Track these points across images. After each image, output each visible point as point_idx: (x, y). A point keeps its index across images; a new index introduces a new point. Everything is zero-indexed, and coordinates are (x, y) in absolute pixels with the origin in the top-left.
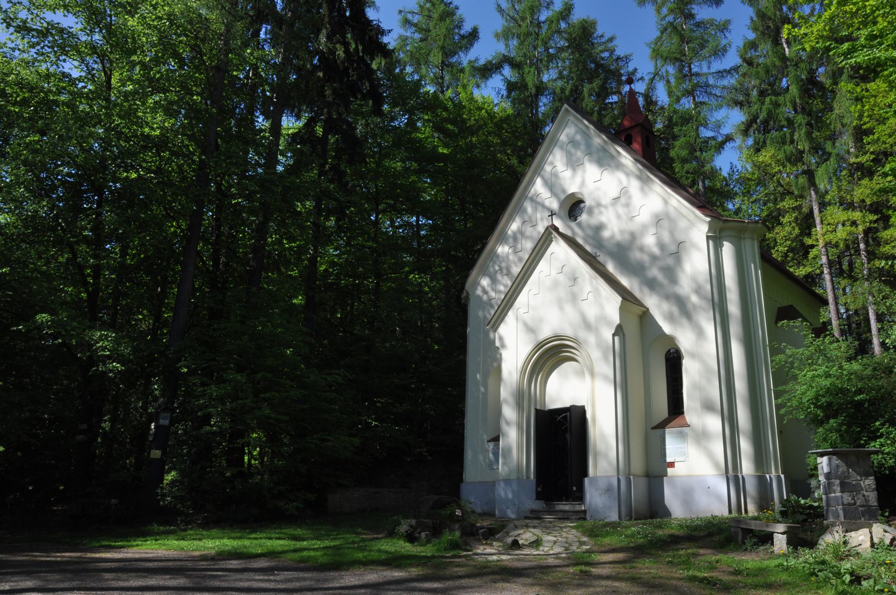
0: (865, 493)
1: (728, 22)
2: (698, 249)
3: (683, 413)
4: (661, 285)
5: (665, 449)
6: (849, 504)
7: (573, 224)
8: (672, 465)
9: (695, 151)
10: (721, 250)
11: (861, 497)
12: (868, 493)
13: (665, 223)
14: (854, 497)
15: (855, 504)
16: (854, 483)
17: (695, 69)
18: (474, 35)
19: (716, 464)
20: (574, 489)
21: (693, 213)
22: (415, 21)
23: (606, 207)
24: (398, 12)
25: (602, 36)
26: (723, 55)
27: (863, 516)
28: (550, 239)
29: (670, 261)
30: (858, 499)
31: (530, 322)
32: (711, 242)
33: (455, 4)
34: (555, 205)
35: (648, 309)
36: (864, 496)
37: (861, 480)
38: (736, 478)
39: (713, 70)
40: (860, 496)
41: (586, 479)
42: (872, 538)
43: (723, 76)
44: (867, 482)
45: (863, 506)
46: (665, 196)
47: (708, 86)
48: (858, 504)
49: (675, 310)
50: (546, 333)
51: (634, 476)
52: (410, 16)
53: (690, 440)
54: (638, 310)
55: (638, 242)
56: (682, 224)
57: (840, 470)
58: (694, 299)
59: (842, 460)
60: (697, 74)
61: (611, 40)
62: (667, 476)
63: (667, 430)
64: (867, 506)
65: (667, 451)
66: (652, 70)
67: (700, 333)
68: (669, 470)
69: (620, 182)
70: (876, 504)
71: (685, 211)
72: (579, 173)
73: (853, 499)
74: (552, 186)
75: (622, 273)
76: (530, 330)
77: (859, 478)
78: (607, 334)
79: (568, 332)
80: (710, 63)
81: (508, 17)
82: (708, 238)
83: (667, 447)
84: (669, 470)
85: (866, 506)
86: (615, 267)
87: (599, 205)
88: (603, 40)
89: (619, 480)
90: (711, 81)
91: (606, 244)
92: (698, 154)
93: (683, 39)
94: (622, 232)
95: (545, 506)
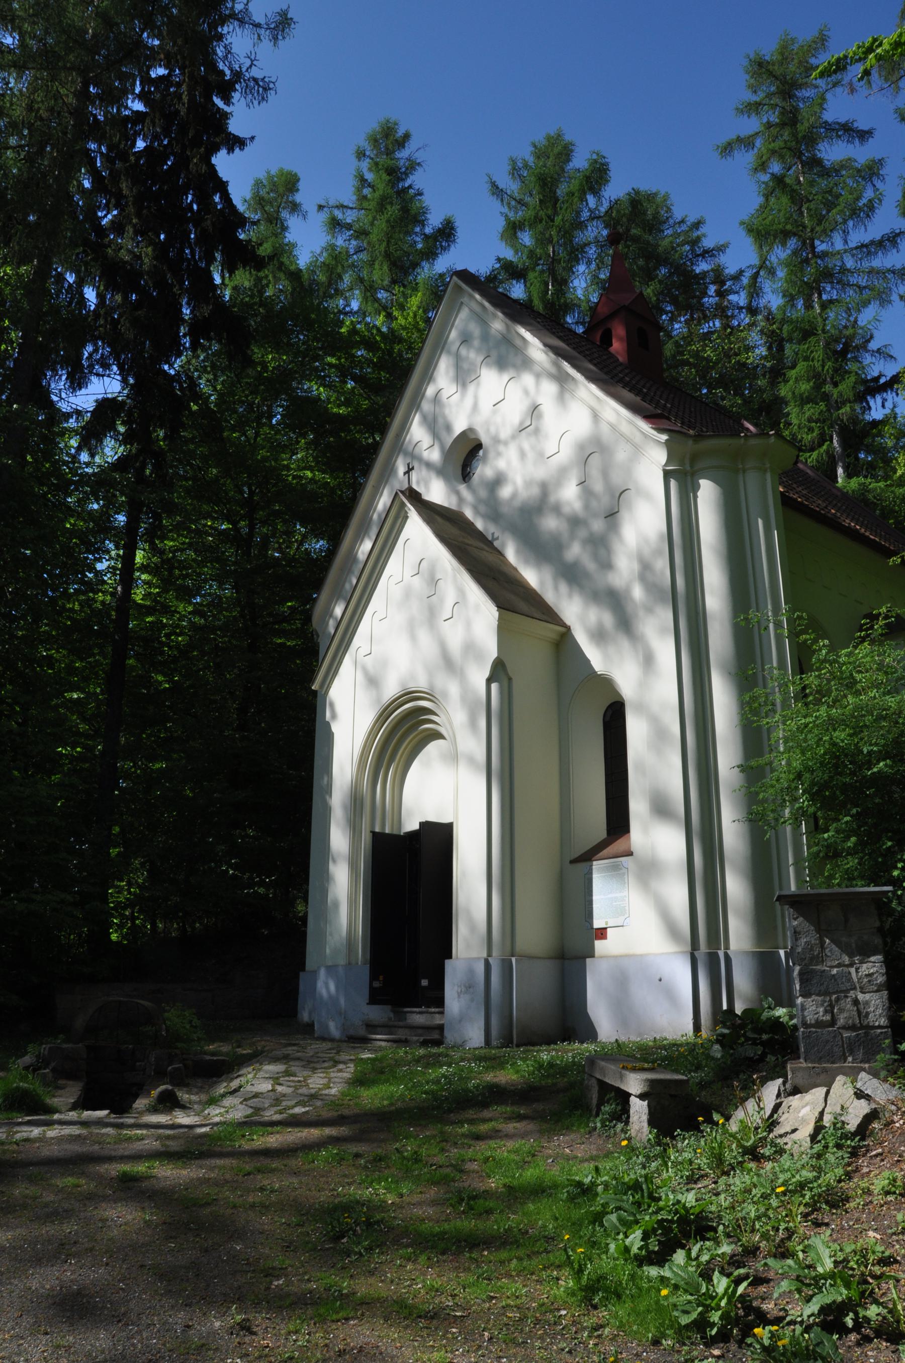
0: (861, 997)
1: (880, 162)
2: (648, 497)
3: (627, 831)
4: (586, 575)
5: (590, 903)
6: (819, 1024)
7: (462, 488)
8: (602, 933)
9: (824, 382)
10: (696, 497)
11: (849, 1006)
12: (867, 996)
13: (595, 460)
14: (832, 1006)
15: (833, 1022)
16: (835, 971)
17: (821, 247)
18: (447, 232)
19: (672, 930)
20: (425, 983)
21: (631, 422)
22: (349, 221)
23: (506, 443)
24: (316, 208)
25: (683, 221)
26: (868, 216)
27: (852, 1052)
28: (402, 514)
29: (598, 525)
30: (841, 1010)
31: (370, 667)
32: (673, 483)
33: (417, 187)
34: (435, 456)
35: (568, 628)
36: (856, 1002)
37: (851, 965)
38: (713, 960)
39: (852, 245)
40: (848, 1004)
41: (447, 962)
42: (822, 1114)
43: (869, 253)
44: (865, 969)
45: (853, 1028)
46: (594, 403)
47: (844, 270)
48: (841, 1022)
49: (608, 619)
50: (391, 689)
51: (522, 957)
52: (338, 214)
53: (632, 880)
54: (550, 631)
55: (552, 499)
56: (621, 454)
57: (803, 941)
58: (638, 593)
59: (807, 918)
60: (824, 255)
61: (697, 225)
62: (592, 956)
63: (596, 865)
64: (862, 1027)
65: (595, 906)
66: (755, 260)
67: (648, 661)
68: (598, 944)
69: (526, 392)
70: (883, 1021)
71: (625, 428)
72: (471, 388)
73: (830, 1010)
74: (435, 426)
75: (526, 562)
76: (373, 681)
77: (846, 959)
78: (478, 676)
79: (421, 683)
80: (846, 233)
81: (513, 203)
82: (667, 475)
83: (594, 898)
84: (598, 944)
85: (861, 1027)
86: (518, 552)
87: (497, 440)
88: (684, 227)
89: (488, 966)
90: (850, 263)
91: (505, 510)
92: (828, 388)
93: (797, 199)
94: (528, 484)
95: (392, 1015)
